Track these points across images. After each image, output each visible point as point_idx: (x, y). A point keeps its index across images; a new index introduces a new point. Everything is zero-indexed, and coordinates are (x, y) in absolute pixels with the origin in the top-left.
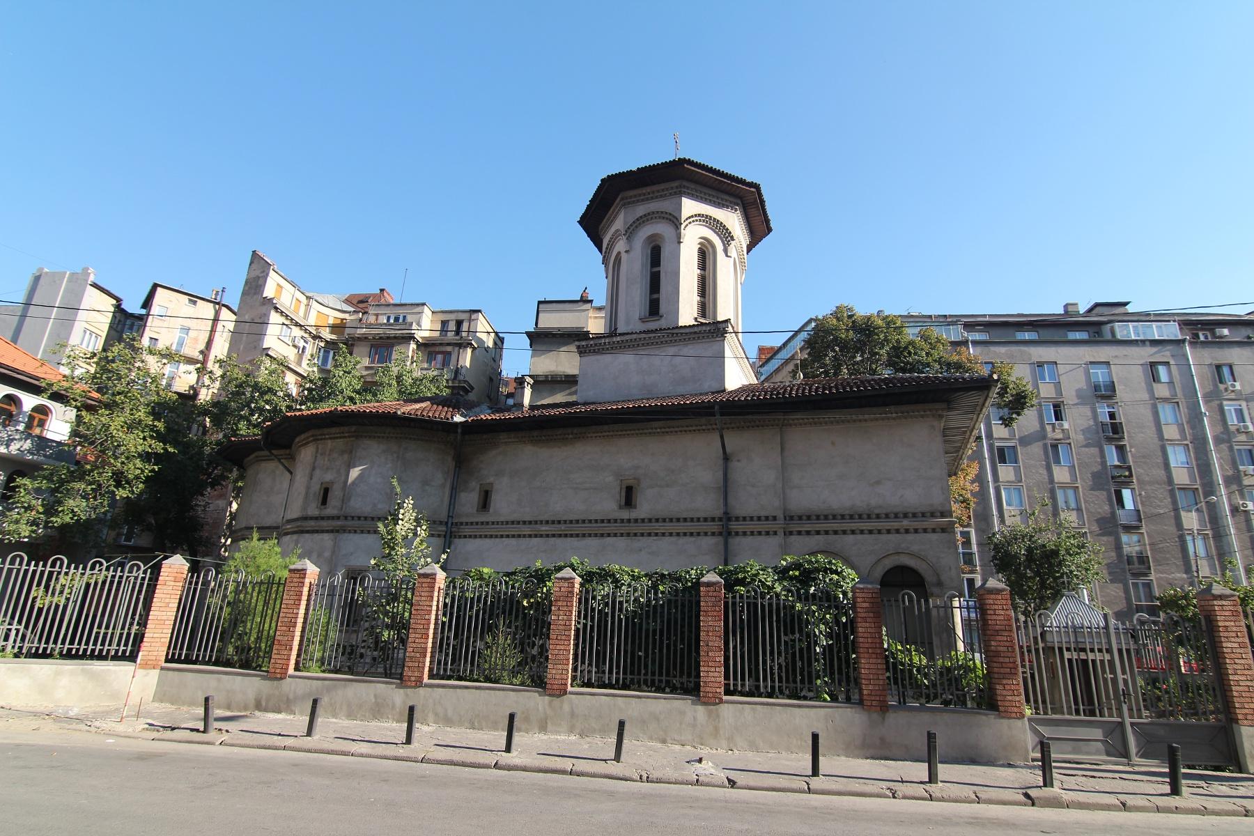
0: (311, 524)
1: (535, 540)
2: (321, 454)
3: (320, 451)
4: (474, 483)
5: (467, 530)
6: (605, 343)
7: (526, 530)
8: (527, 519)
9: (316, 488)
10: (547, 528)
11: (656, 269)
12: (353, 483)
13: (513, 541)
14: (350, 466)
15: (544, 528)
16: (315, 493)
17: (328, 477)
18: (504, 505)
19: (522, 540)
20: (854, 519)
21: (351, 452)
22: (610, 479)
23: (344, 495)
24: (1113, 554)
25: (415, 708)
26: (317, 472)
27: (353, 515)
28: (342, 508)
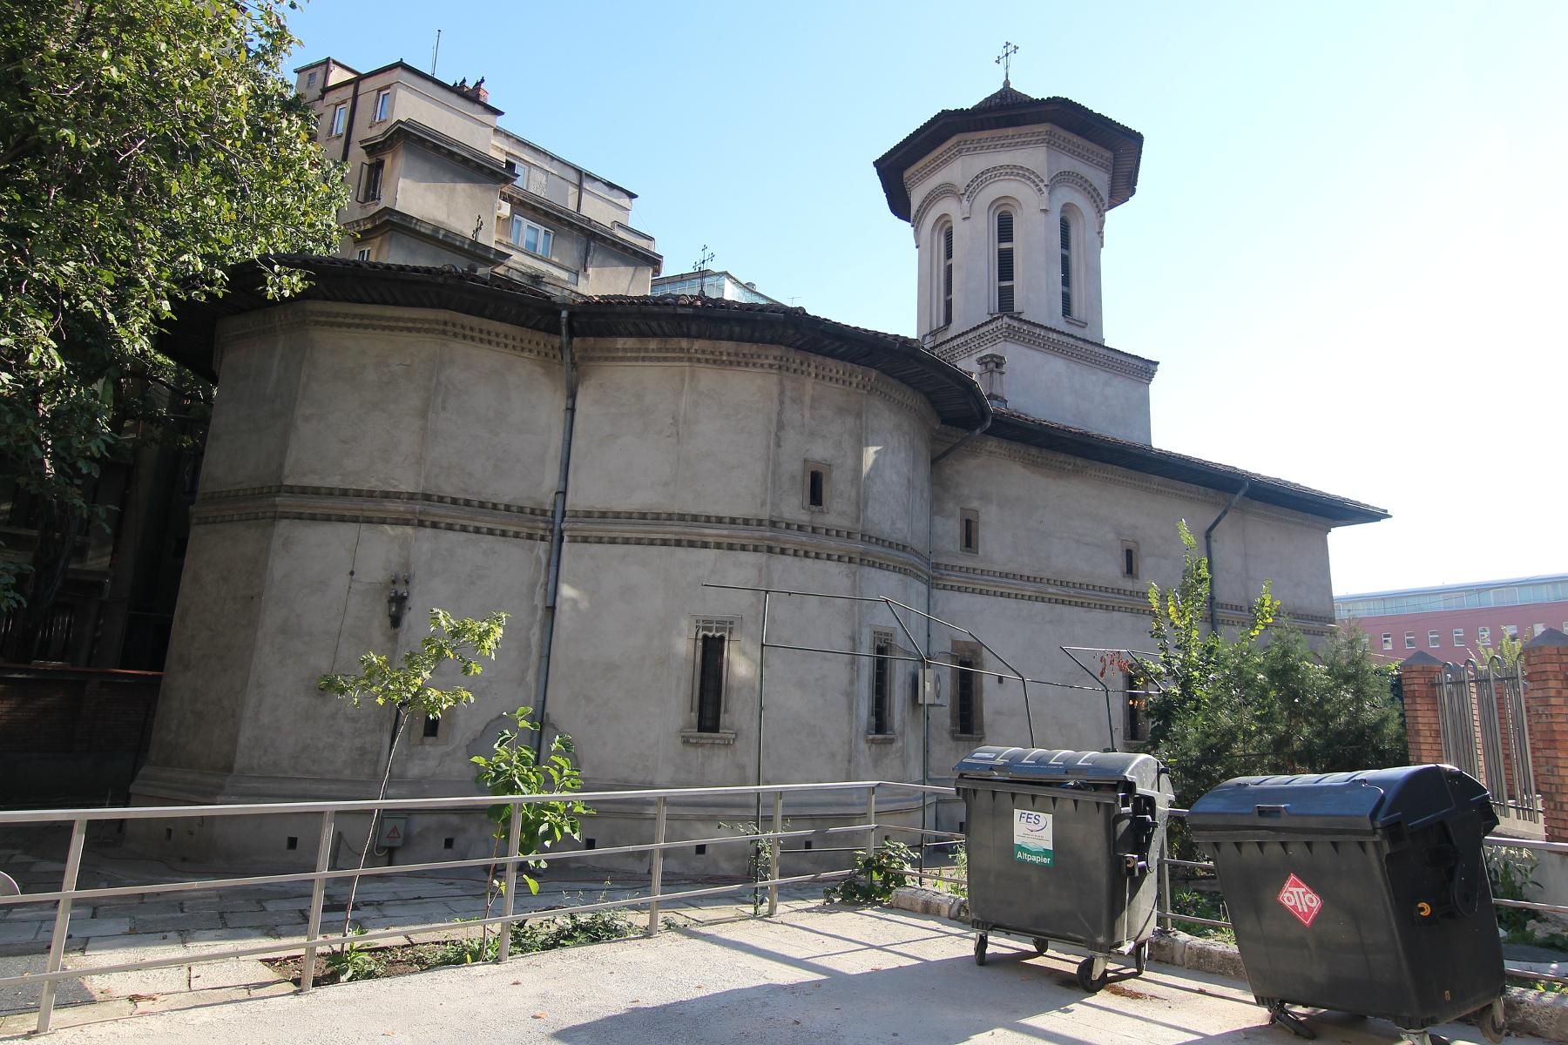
0: (793, 539)
1: (1039, 605)
2: (794, 401)
3: (788, 393)
4: (951, 505)
5: (954, 579)
6: (1039, 335)
7: (1029, 589)
8: (1026, 573)
9: (793, 467)
10: (1055, 591)
11: (1005, 245)
12: (868, 476)
13: (1011, 603)
14: (860, 444)
15: (1051, 590)
16: (793, 477)
17: (820, 451)
18: (996, 547)
19: (1024, 604)
20: (709, 522)
21: (859, 415)
22: (1111, 536)
23: (858, 494)
24: (95, 464)
25: (455, 841)
26: (791, 439)
27: (872, 534)
28: (858, 519)
